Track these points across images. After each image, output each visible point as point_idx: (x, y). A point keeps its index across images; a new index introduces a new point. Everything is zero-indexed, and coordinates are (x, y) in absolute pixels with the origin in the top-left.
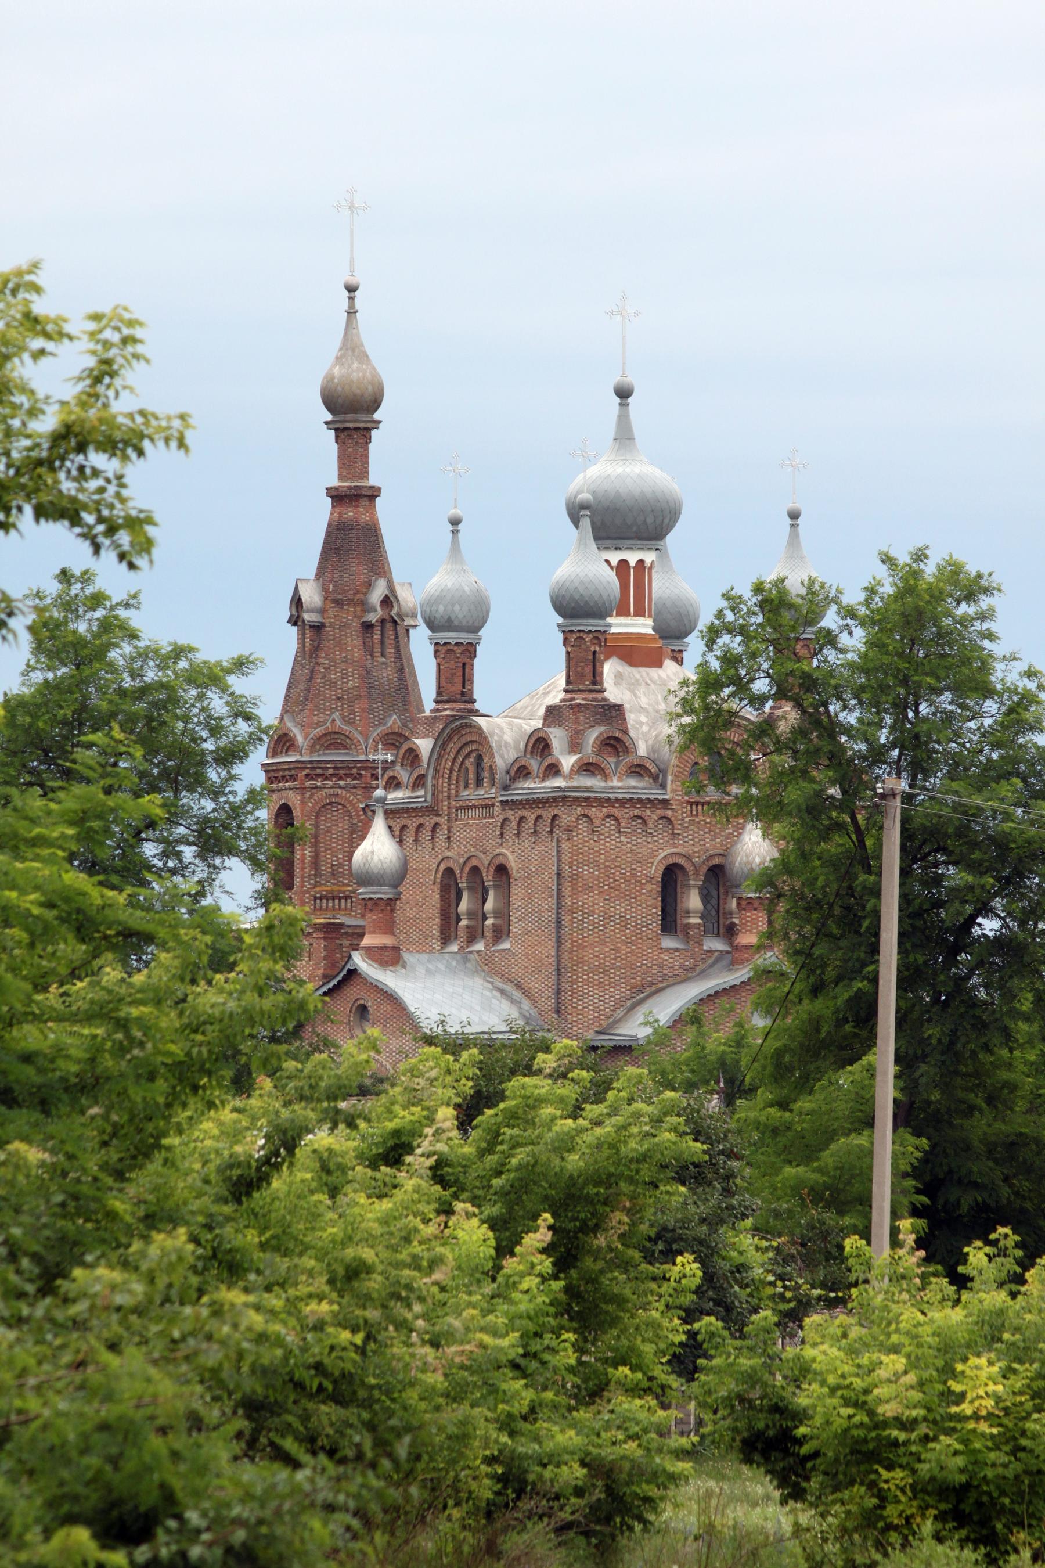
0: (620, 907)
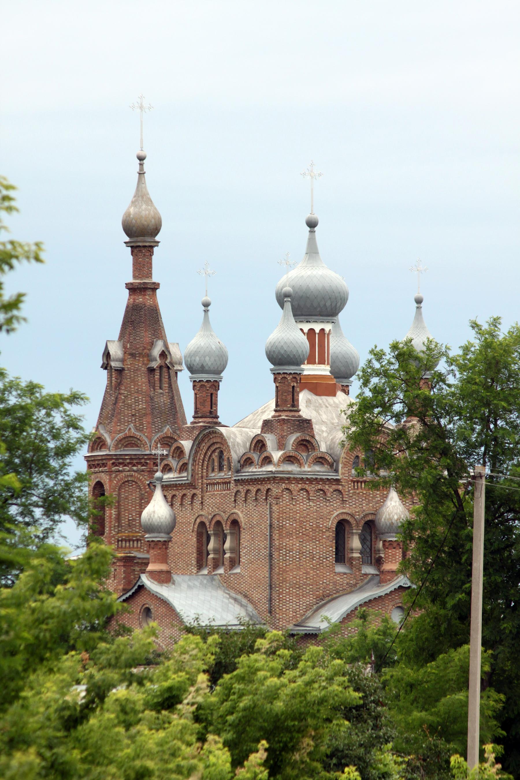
0: (309, 547)
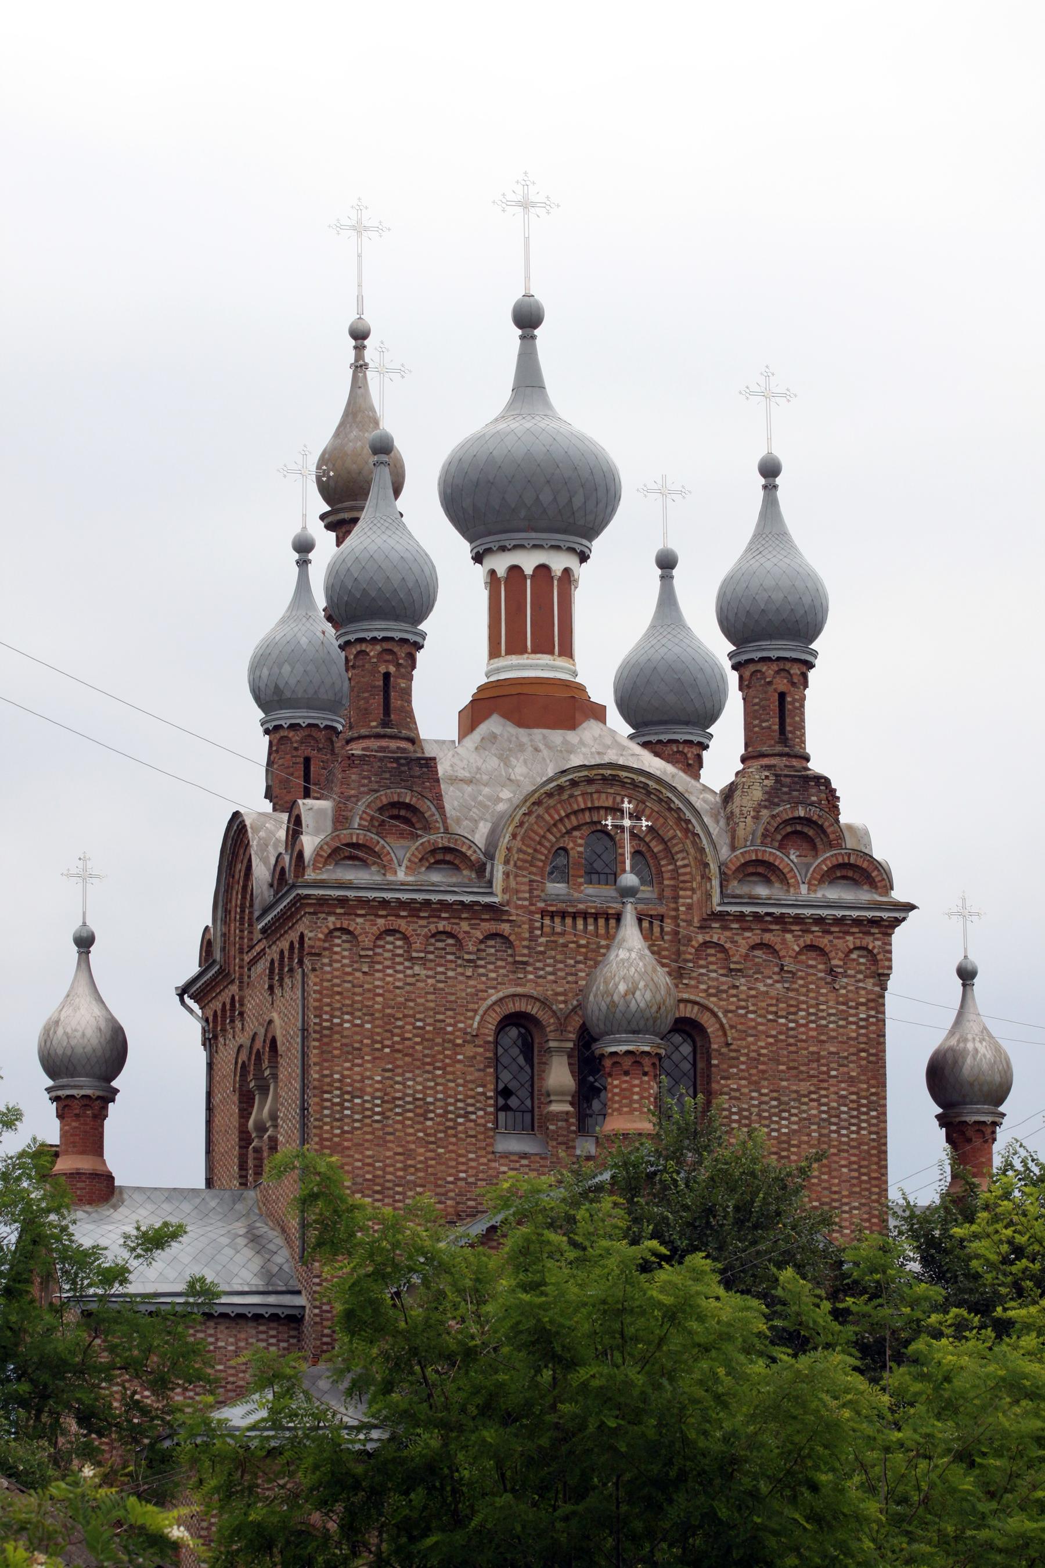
0: (414, 1084)
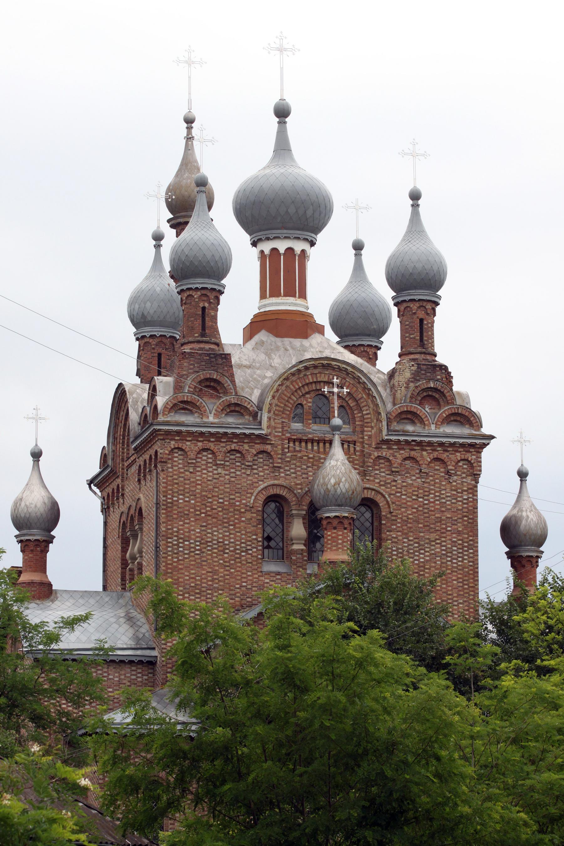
0: (218, 534)
